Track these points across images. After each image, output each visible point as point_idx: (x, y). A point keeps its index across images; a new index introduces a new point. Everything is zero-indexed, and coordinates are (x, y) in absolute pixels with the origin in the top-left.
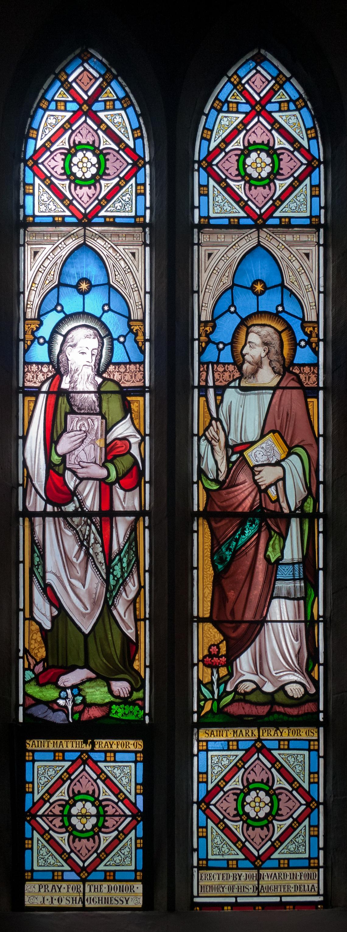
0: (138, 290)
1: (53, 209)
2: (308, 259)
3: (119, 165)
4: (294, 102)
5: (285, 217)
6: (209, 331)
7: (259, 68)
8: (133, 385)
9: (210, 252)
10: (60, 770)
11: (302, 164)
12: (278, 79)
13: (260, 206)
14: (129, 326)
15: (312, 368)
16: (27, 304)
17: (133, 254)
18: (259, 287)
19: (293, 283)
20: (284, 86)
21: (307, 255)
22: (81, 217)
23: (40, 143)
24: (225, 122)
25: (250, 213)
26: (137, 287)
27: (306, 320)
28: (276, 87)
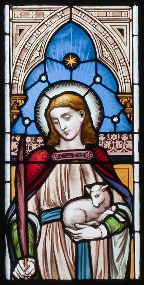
0: (126, 65)
2: (123, 35)
8: (119, 153)
9: (21, 28)
14: (118, 99)
16: (13, 80)
17: (121, 31)
18: (71, 61)
21: (121, 31)
26: (125, 61)
27: (120, 91)
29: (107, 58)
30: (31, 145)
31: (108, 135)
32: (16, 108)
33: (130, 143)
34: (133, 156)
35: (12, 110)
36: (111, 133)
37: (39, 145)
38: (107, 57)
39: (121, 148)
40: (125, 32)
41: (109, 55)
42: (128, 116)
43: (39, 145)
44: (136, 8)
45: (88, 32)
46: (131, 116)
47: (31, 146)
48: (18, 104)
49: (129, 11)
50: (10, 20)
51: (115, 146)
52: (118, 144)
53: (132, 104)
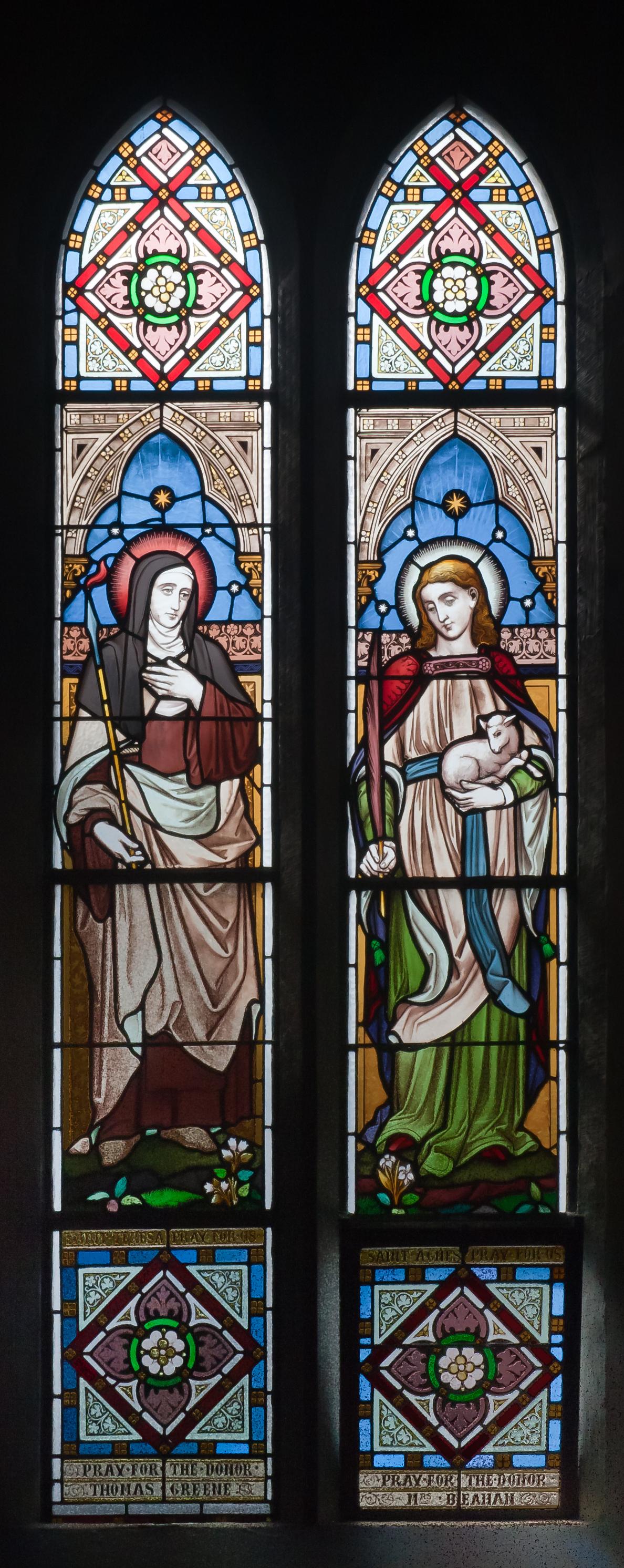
0: (547, 509)
1: (402, 369)
3: (510, 292)
4: (517, 190)
5: (204, 379)
7: (166, 131)
8: (534, 660)
10: (419, 1298)
11: (527, 291)
12: (198, 149)
13: (454, 360)
14: (238, 563)
19: (220, 491)
20: (208, 160)
22: (446, 379)
23: (87, 258)
24: (399, 219)
25: (147, 373)
28: (491, 163)
31: (517, 630)
32: (71, 578)
33: (551, 643)
36: (520, 627)
48: (75, 571)
49: (550, 416)
51: (527, 649)
52: (533, 645)
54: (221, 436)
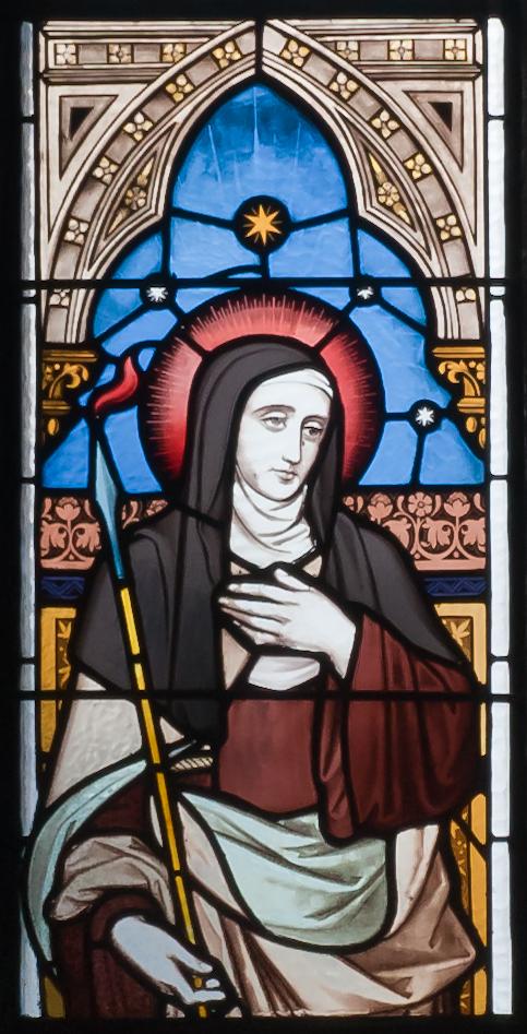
0: (463, 238)
6: (76, 383)
14: (431, 363)
15: (438, 498)
17: (444, 110)
19: (390, 209)
21: (444, 110)
26: (459, 224)
27: (441, 334)
29: (390, 209)
30: (424, 526)
31: (401, 498)
32: (58, 393)
34: (484, 575)
35: (44, 403)
37: (454, 523)
38: (390, 202)
39: (58, 548)
40: (456, 111)
41: (397, 198)
42: (470, 425)
43: (454, 523)
44: (496, 28)
45: (320, 116)
46: (479, 427)
47: (427, 530)
48: (69, 379)
49: (470, 37)
50: (37, 76)
52: (436, 530)
53: (484, 382)
54: (393, 90)
